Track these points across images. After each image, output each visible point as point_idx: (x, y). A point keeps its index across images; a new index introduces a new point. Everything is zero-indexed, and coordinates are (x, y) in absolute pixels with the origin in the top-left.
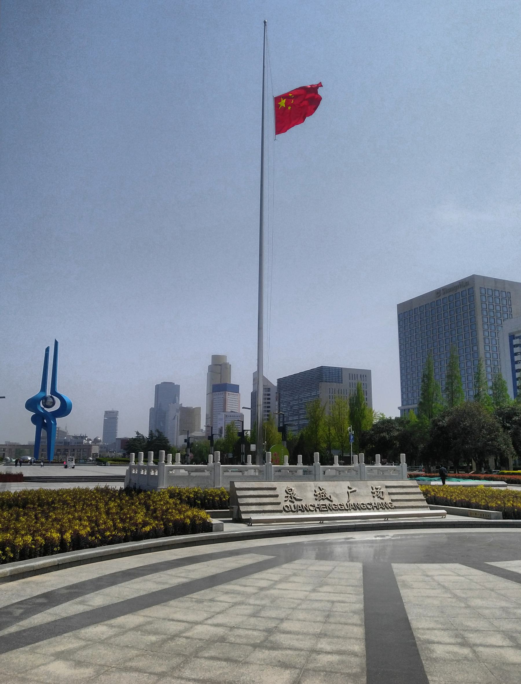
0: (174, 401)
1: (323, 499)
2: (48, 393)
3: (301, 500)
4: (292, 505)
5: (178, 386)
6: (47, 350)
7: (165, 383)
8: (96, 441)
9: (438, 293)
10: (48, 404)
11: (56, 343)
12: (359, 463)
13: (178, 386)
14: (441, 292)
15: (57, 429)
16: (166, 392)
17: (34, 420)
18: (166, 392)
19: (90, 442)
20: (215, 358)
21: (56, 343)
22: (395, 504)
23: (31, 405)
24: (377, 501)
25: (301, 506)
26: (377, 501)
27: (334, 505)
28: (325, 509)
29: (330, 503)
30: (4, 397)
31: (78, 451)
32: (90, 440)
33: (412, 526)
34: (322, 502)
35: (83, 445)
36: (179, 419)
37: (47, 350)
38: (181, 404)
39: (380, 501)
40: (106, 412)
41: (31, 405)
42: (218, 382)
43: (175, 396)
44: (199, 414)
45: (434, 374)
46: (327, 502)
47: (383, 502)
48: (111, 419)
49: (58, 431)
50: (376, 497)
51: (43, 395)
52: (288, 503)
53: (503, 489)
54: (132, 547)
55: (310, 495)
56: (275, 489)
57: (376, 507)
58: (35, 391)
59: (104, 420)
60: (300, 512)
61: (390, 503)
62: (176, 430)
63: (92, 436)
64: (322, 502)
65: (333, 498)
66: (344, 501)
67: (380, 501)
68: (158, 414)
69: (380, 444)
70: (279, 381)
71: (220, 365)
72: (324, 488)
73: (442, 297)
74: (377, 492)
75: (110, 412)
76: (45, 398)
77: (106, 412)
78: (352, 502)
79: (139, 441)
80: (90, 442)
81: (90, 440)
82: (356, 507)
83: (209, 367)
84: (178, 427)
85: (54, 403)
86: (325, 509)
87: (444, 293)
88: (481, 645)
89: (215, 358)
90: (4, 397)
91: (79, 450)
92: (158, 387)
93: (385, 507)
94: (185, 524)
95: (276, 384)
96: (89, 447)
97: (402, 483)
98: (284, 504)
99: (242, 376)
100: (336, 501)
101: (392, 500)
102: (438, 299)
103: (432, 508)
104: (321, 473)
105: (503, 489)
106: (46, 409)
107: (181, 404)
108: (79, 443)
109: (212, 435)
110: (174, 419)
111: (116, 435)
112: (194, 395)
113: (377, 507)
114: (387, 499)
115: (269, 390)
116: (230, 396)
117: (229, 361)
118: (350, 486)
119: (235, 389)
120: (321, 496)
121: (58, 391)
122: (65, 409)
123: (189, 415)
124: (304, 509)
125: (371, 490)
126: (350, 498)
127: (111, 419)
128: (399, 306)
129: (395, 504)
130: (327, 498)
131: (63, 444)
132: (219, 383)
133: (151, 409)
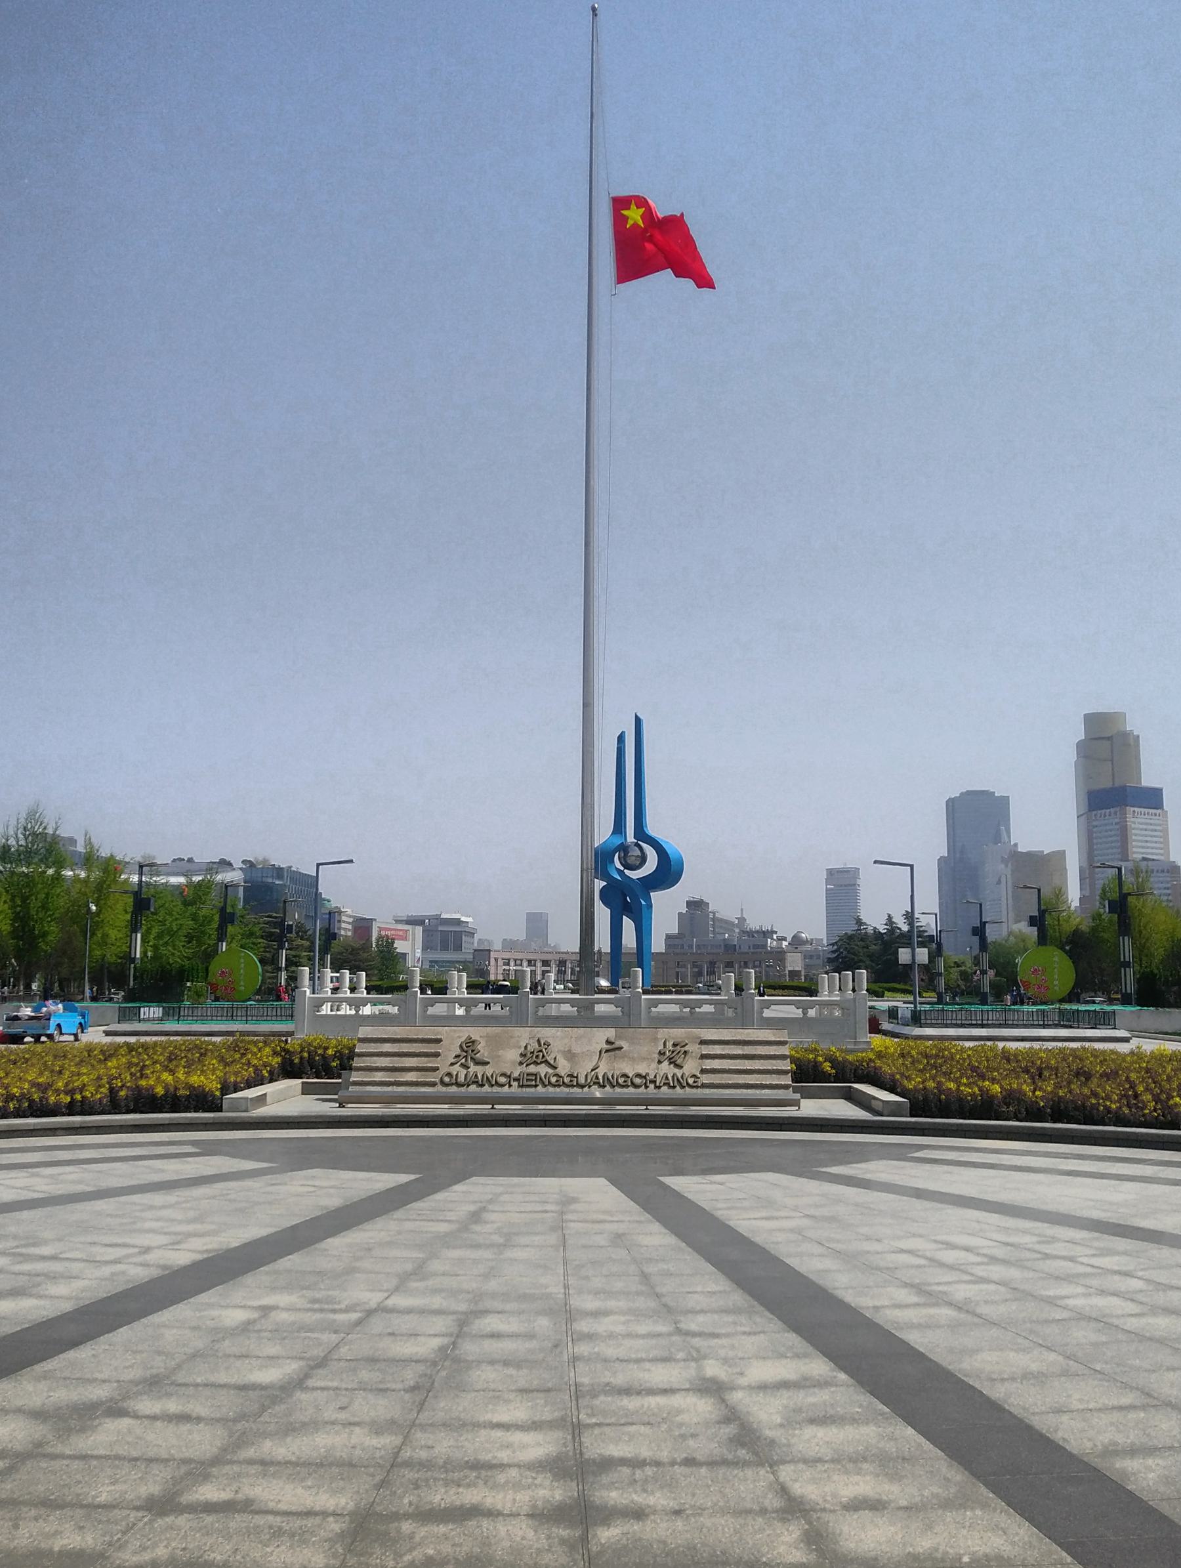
0: (997, 839)
1: (536, 1063)
2: (631, 839)
5: (1005, 800)
6: (621, 739)
7: (969, 793)
8: (797, 941)
10: (630, 861)
11: (638, 721)
12: (854, 990)
13: (1005, 800)
15: (711, 916)
16: (975, 818)
18: (975, 818)
19: (785, 944)
20: (1093, 721)
21: (638, 721)
22: (705, 1079)
26: (666, 1068)
27: (556, 1075)
29: (551, 1071)
30: (351, 861)
32: (784, 939)
33: (1030, 1135)
34: (532, 1069)
35: (767, 952)
36: (1010, 884)
37: (621, 739)
38: (1016, 845)
40: (830, 872)
42: (1105, 783)
43: (999, 825)
44: (1063, 870)
48: (842, 886)
49: (713, 919)
50: (666, 1063)
51: (618, 841)
53: (1123, 1048)
54: (8, 1125)
55: (513, 1055)
56: (438, 1041)
59: (827, 890)
61: (694, 1076)
62: (1004, 907)
63: (786, 930)
64: (532, 1069)
68: (958, 873)
71: (1109, 738)
76: (624, 849)
77: (830, 872)
79: (862, 940)
80: (785, 944)
81: (784, 939)
83: (1079, 745)
84: (1010, 901)
85: (643, 859)
88: (1131, 1408)
89: (1093, 721)
90: (351, 861)
91: (757, 963)
92: (952, 805)
94: (154, 1097)
96: (780, 955)
97: (748, 1034)
105: (1123, 1048)
106: (625, 874)
107: (1016, 845)
108: (756, 946)
109: (983, 924)
110: (999, 882)
112: (1048, 823)
116: (1137, 819)
117: (1133, 725)
121: (651, 830)
123: (1036, 867)
127: (842, 886)
129: (705, 1079)
130: (546, 1062)
131: (722, 950)
132: (1109, 785)
133: (941, 860)
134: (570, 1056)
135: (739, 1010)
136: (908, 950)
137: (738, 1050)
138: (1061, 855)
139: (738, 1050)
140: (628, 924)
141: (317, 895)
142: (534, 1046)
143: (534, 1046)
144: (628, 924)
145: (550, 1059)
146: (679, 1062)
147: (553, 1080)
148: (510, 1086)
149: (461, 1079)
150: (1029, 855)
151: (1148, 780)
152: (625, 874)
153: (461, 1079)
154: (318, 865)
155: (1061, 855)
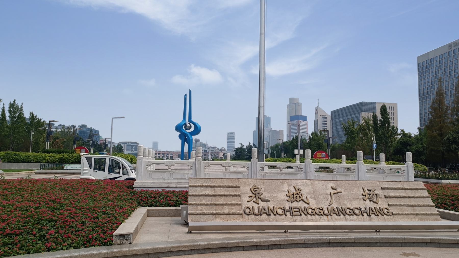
3: (269, 201)
4: (256, 206)
6: (186, 95)
9: (449, 46)
10: (187, 128)
11: (190, 91)
14: (453, 45)
17: (180, 137)
20: (291, 99)
21: (190, 91)
23: (178, 128)
24: (369, 204)
25: (266, 209)
26: (369, 204)
28: (298, 213)
29: (306, 206)
30: (124, 117)
31: (212, 155)
34: (295, 204)
37: (186, 95)
39: (373, 205)
40: (228, 133)
41: (178, 128)
45: (445, 100)
46: (302, 205)
47: (377, 206)
48: (231, 137)
50: (368, 201)
52: (251, 204)
55: (283, 196)
57: (366, 212)
58: (179, 120)
60: (264, 216)
64: (295, 204)
65: (311, 201)
66: (324, 205)
67: (373, 205)
69: (393, 147)
70: (333, 112)
72: (301, 187)
73: (453, 49)
74: (370, 194)
75: (231, 133)
77: (228, 133)
78: (335, 206)
82: (341, 212)
85: (190, 127)
86: (298, 213)
87: (455, 46)
89: (291, 99)
90: (124, 117)
93: (379, 212)
95: (330, 114)
98: (245, 204)
99: (308, 111)
100: (313, 204)
101: (389, 205)
102: (449, 50)
103: (443, 216)
104: (259, 169)
106: (187, 132)
111: (234, 146)
113: (369, 213)
114: (382, 204)
115: (326, 118)
117: (300, 101)
118: (334, 187)
119: (305, 118)
120: (296, 196)
121: (193, 119)
122: (197, 130)
124: (269, 212)
125: (362, 192)
126: (334, 201)
127: (231, 137)
128: (419, 58)
134: (316, 195)
135: (249, 168)
136: (297, 150)
137: (402, 193)
138: (282, 131)
139: (402, 193)
140: (186, 144)
141: (99, 135)
142: (293, 191)
143: (293, 191)
144: (186, 144)
145: (304, 198)
146: (375, 200)
147: (310, 211)
148: (286, 215)
149: (256, 211)
150: (275, 131)
151: (303, 114)
152: (187, 132)
153: (256, 211)
154: (113, 118)
155: (282, 131)
